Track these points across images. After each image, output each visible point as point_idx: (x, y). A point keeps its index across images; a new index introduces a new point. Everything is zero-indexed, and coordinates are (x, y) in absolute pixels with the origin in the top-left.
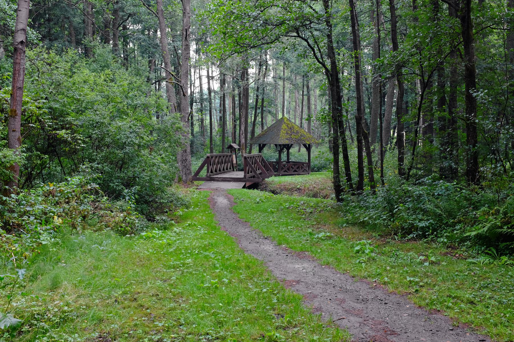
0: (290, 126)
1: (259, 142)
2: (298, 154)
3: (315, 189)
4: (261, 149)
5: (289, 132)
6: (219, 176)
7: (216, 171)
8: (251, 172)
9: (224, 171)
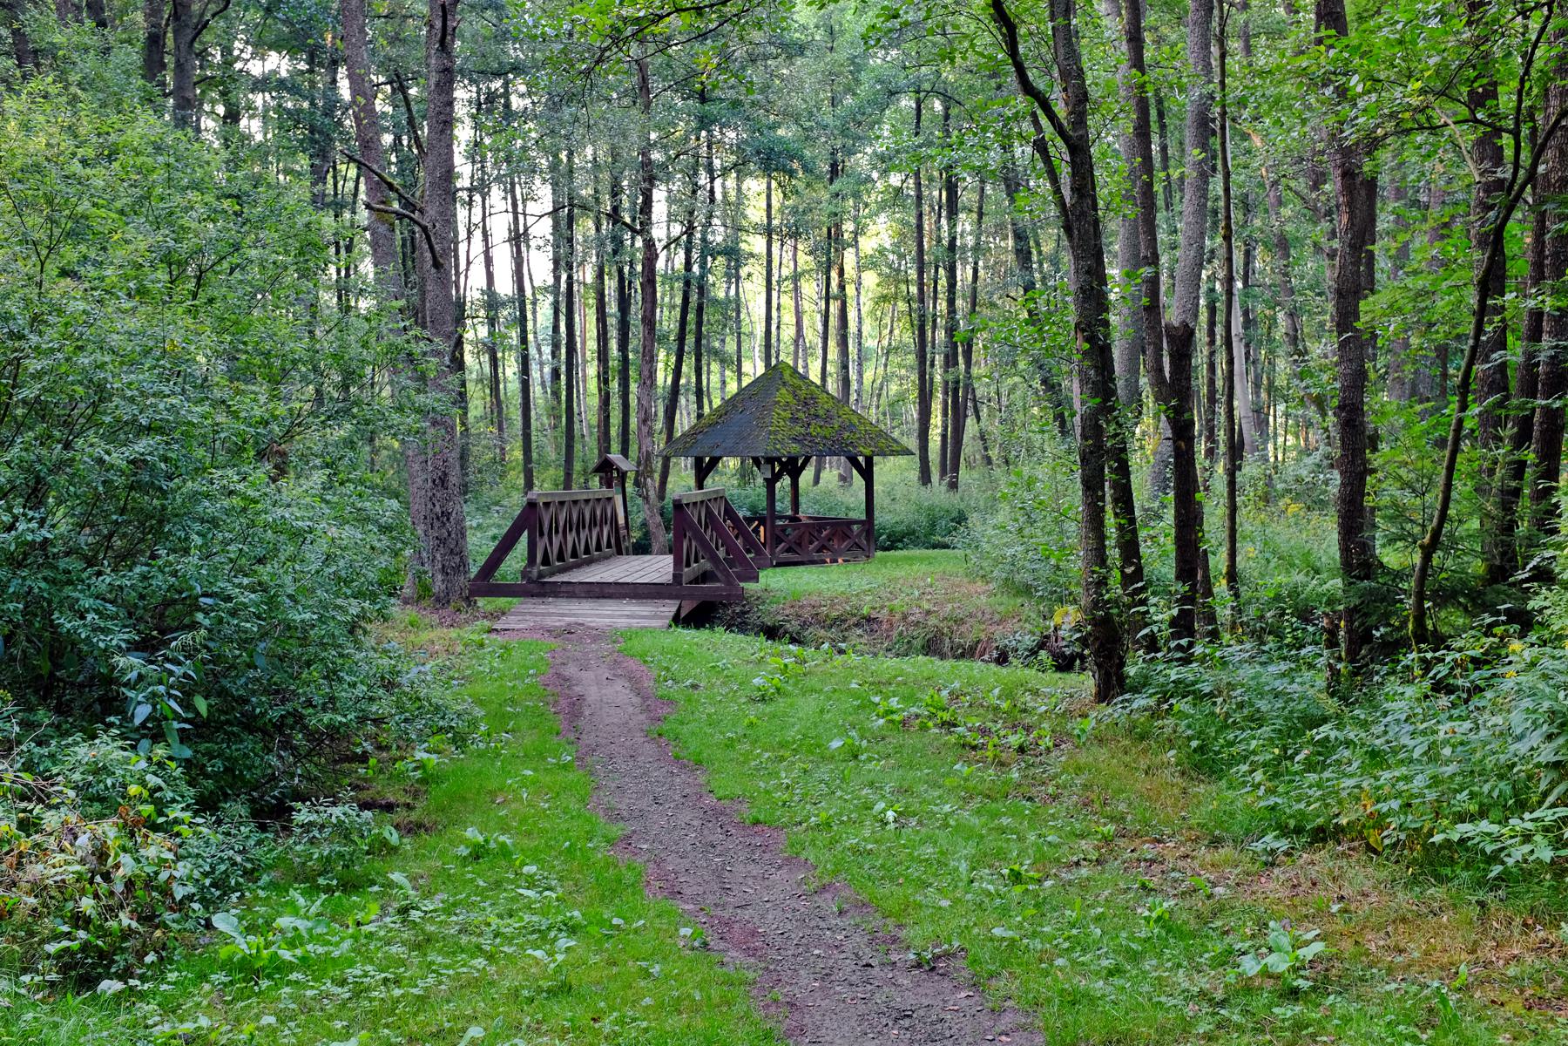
0: (802, 394)
1: (698, 451)
2: (827, 488)
3: (932, 621)
4: (703, 470)
5: (801, 415)
6: (564, 578)
7: (561, 557)
8: (696, 561)
9: (589, 557)
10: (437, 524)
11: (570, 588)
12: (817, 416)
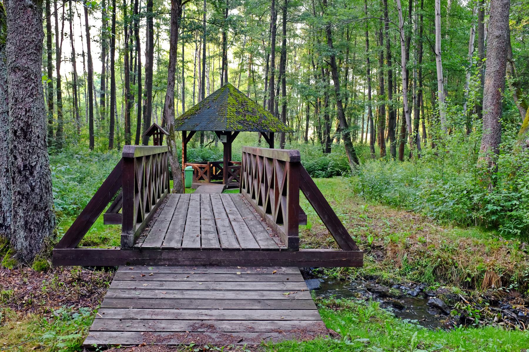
0: (240, 99)
5: (241, 110)
10: (18, 178)
11: (172, 255)
12: (248, 111)
